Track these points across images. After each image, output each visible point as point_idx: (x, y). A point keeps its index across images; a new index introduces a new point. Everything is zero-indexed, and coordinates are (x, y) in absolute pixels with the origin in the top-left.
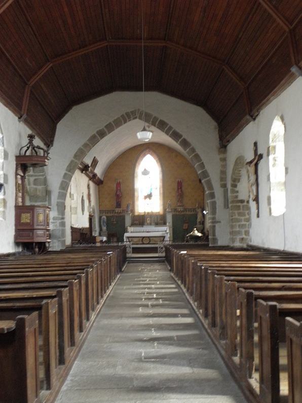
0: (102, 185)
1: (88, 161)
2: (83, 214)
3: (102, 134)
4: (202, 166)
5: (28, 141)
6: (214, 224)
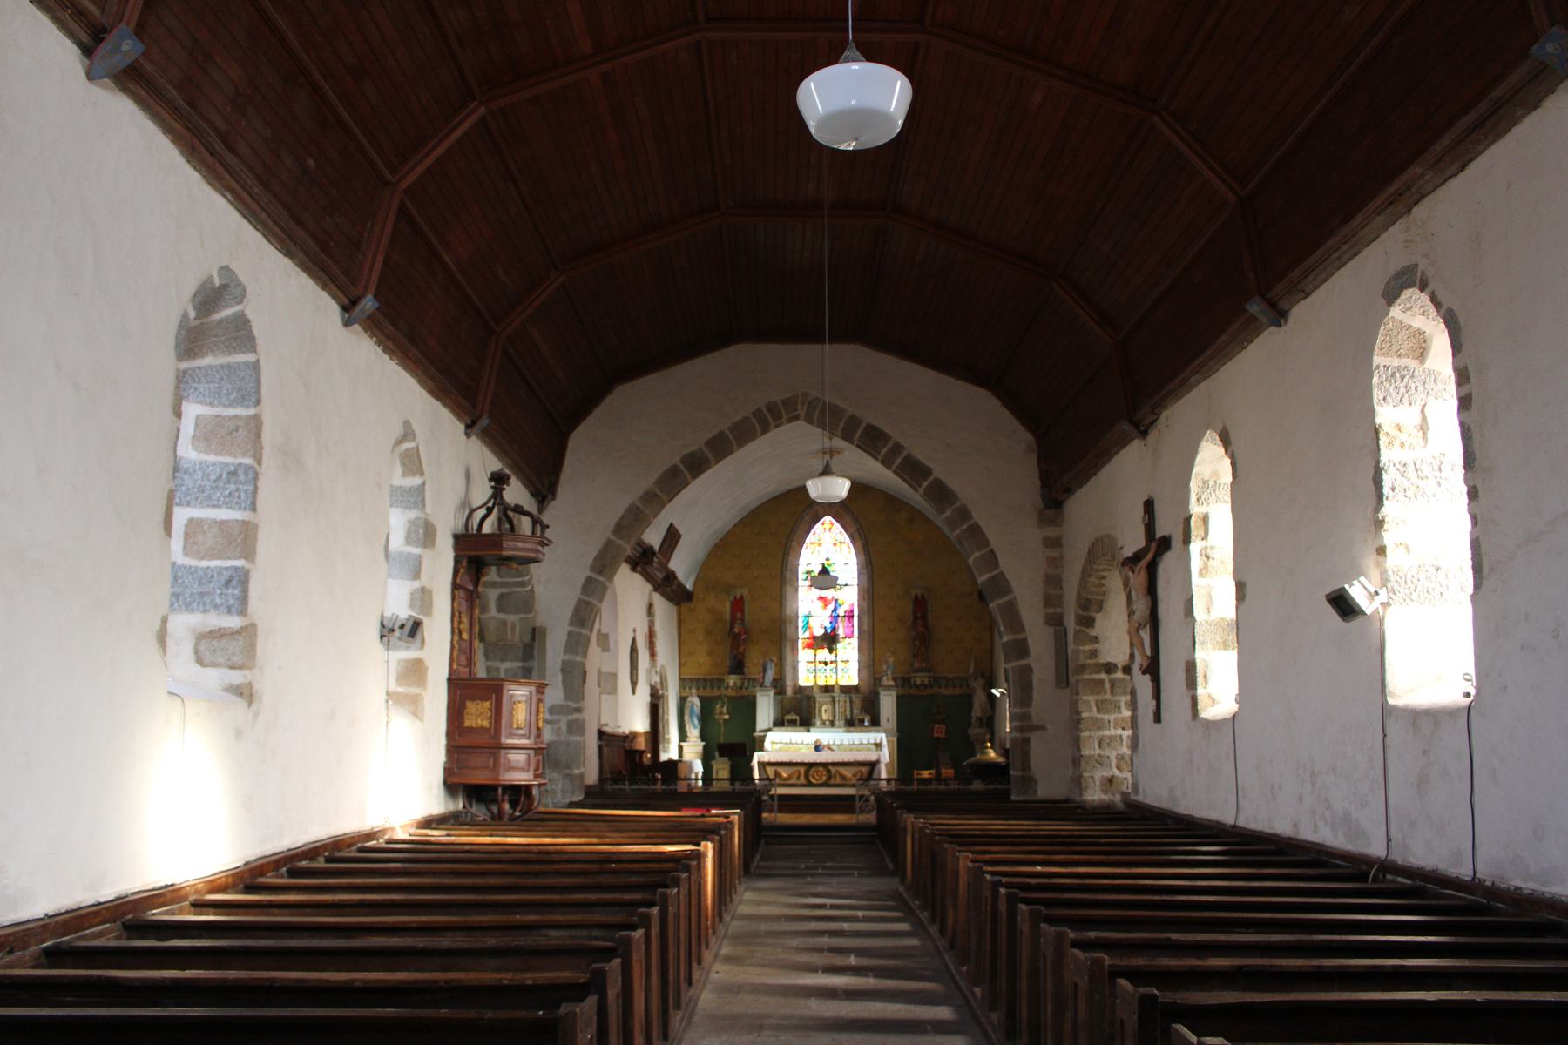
0: (691, 605)
1: (653, 537)
2: (634, 693)
3: (696, 465)
4: (991, 560)
5: (489, 492)
6: (1027, 735)
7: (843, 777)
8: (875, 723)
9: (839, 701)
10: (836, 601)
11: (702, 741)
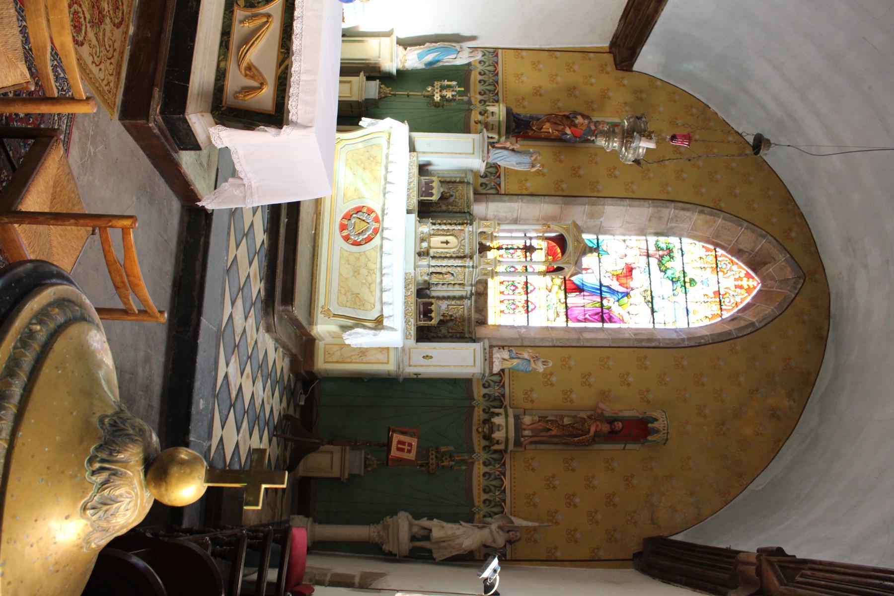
0: (611, 68)
7: (249, 39)
8: (424, 334)
10: (627, 294)
11: (398, 71)
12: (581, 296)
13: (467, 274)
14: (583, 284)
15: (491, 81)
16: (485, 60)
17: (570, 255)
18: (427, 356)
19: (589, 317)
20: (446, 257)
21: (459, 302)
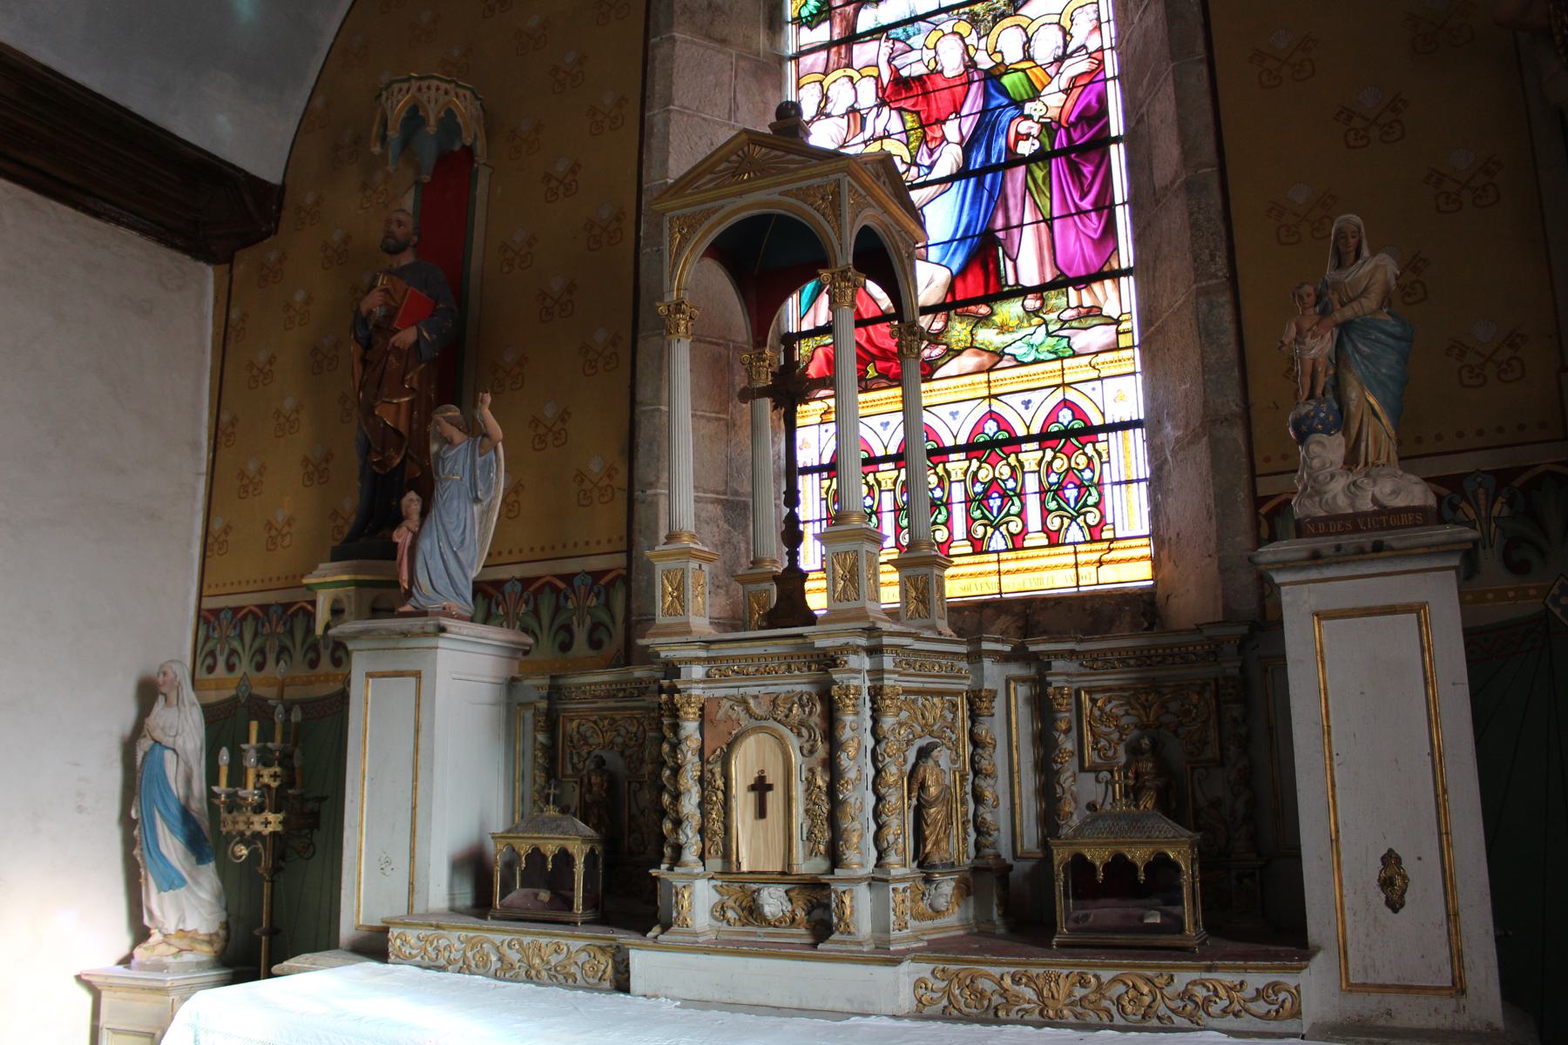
9: (384, 139)
12: (1009, 237)
13: (916, 683)
14: (962, 240)
15: (280, 629)
16: (226, 651)
17: (796, 194)
18: (1386, 883)
19: (1091, 197)
20: (832, 791)
21: (1065, 717)
